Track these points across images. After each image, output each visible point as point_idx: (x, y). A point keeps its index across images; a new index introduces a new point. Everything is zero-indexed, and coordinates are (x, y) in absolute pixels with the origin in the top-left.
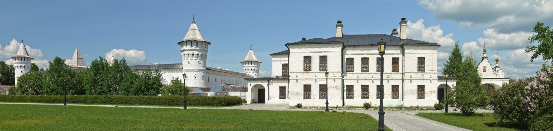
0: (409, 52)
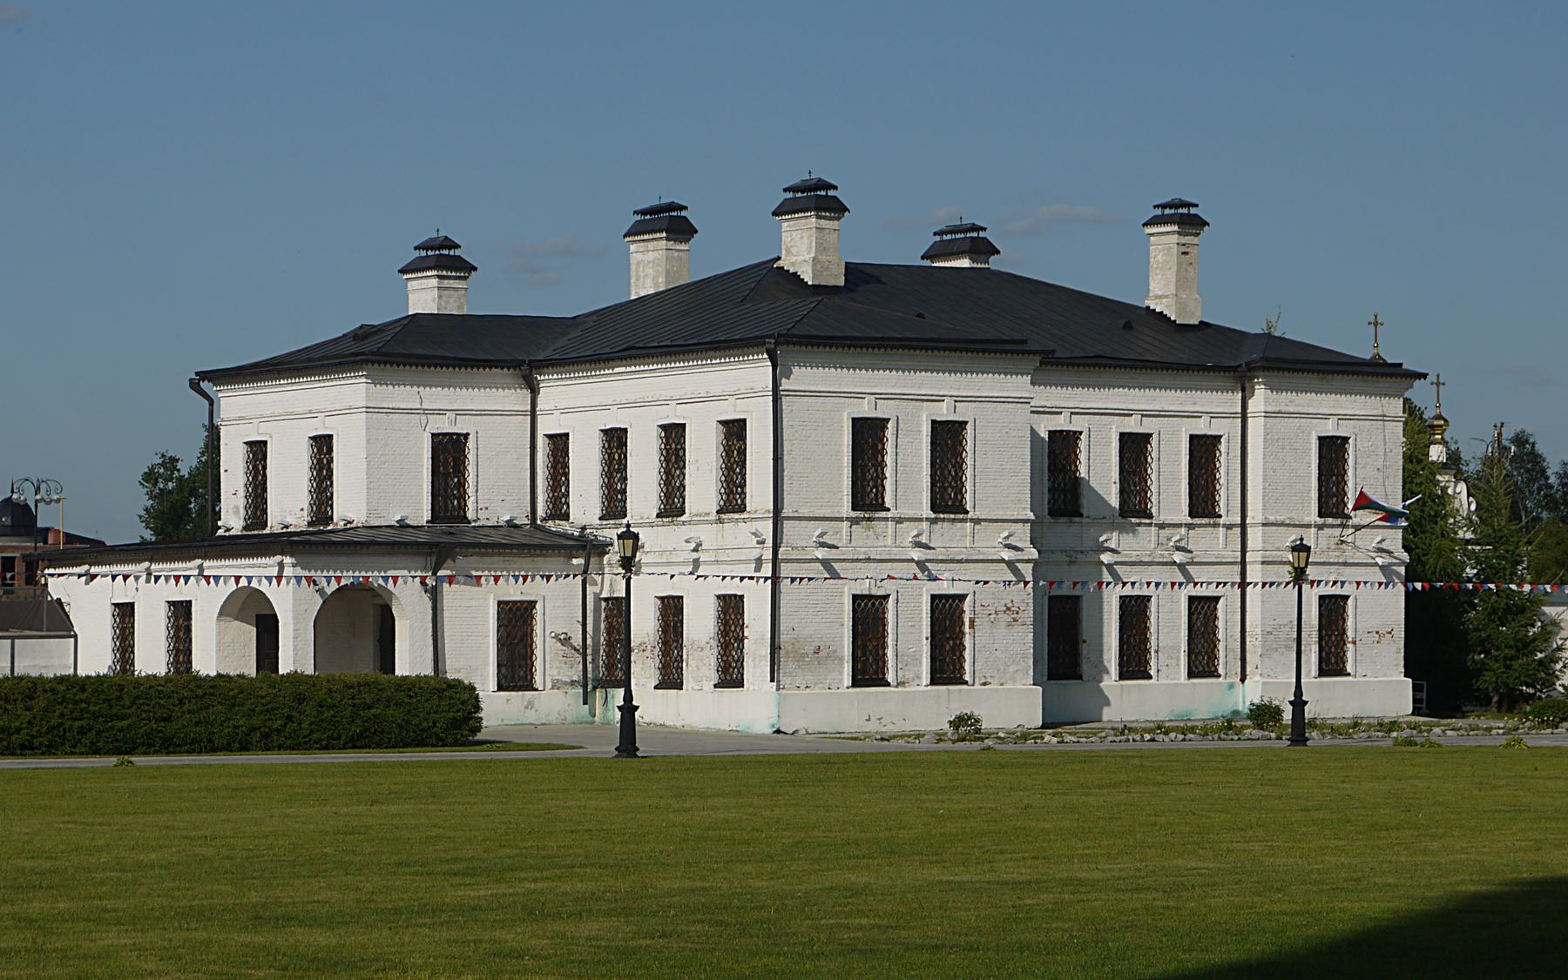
0: (1284, 409)
